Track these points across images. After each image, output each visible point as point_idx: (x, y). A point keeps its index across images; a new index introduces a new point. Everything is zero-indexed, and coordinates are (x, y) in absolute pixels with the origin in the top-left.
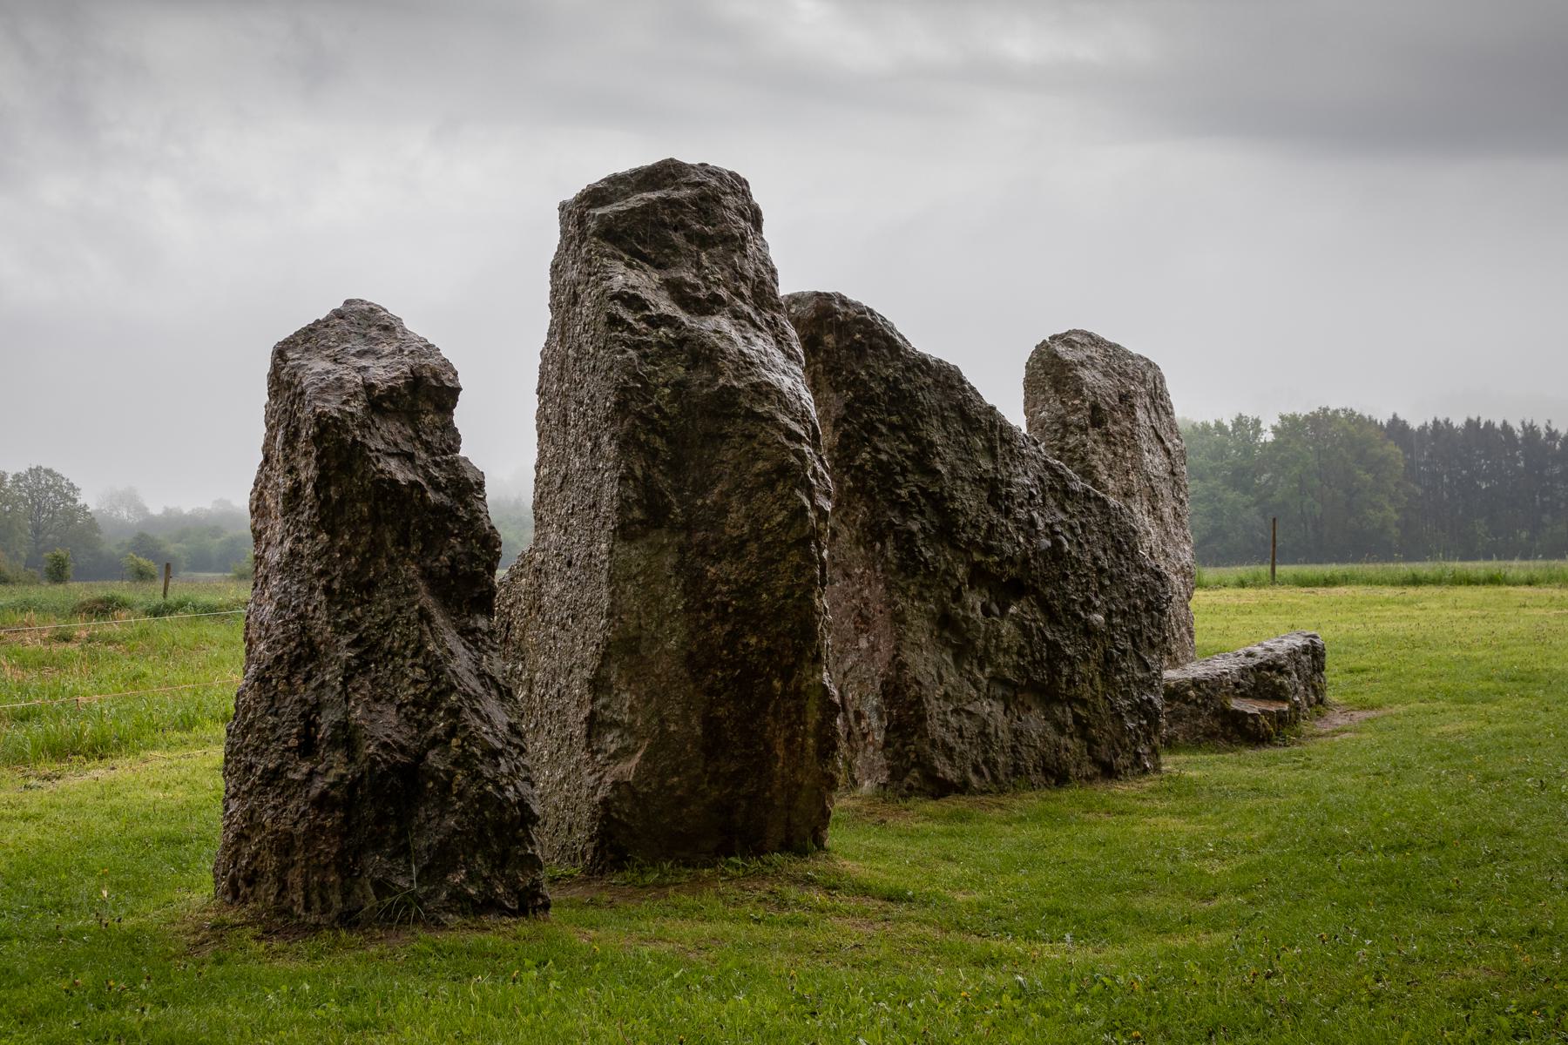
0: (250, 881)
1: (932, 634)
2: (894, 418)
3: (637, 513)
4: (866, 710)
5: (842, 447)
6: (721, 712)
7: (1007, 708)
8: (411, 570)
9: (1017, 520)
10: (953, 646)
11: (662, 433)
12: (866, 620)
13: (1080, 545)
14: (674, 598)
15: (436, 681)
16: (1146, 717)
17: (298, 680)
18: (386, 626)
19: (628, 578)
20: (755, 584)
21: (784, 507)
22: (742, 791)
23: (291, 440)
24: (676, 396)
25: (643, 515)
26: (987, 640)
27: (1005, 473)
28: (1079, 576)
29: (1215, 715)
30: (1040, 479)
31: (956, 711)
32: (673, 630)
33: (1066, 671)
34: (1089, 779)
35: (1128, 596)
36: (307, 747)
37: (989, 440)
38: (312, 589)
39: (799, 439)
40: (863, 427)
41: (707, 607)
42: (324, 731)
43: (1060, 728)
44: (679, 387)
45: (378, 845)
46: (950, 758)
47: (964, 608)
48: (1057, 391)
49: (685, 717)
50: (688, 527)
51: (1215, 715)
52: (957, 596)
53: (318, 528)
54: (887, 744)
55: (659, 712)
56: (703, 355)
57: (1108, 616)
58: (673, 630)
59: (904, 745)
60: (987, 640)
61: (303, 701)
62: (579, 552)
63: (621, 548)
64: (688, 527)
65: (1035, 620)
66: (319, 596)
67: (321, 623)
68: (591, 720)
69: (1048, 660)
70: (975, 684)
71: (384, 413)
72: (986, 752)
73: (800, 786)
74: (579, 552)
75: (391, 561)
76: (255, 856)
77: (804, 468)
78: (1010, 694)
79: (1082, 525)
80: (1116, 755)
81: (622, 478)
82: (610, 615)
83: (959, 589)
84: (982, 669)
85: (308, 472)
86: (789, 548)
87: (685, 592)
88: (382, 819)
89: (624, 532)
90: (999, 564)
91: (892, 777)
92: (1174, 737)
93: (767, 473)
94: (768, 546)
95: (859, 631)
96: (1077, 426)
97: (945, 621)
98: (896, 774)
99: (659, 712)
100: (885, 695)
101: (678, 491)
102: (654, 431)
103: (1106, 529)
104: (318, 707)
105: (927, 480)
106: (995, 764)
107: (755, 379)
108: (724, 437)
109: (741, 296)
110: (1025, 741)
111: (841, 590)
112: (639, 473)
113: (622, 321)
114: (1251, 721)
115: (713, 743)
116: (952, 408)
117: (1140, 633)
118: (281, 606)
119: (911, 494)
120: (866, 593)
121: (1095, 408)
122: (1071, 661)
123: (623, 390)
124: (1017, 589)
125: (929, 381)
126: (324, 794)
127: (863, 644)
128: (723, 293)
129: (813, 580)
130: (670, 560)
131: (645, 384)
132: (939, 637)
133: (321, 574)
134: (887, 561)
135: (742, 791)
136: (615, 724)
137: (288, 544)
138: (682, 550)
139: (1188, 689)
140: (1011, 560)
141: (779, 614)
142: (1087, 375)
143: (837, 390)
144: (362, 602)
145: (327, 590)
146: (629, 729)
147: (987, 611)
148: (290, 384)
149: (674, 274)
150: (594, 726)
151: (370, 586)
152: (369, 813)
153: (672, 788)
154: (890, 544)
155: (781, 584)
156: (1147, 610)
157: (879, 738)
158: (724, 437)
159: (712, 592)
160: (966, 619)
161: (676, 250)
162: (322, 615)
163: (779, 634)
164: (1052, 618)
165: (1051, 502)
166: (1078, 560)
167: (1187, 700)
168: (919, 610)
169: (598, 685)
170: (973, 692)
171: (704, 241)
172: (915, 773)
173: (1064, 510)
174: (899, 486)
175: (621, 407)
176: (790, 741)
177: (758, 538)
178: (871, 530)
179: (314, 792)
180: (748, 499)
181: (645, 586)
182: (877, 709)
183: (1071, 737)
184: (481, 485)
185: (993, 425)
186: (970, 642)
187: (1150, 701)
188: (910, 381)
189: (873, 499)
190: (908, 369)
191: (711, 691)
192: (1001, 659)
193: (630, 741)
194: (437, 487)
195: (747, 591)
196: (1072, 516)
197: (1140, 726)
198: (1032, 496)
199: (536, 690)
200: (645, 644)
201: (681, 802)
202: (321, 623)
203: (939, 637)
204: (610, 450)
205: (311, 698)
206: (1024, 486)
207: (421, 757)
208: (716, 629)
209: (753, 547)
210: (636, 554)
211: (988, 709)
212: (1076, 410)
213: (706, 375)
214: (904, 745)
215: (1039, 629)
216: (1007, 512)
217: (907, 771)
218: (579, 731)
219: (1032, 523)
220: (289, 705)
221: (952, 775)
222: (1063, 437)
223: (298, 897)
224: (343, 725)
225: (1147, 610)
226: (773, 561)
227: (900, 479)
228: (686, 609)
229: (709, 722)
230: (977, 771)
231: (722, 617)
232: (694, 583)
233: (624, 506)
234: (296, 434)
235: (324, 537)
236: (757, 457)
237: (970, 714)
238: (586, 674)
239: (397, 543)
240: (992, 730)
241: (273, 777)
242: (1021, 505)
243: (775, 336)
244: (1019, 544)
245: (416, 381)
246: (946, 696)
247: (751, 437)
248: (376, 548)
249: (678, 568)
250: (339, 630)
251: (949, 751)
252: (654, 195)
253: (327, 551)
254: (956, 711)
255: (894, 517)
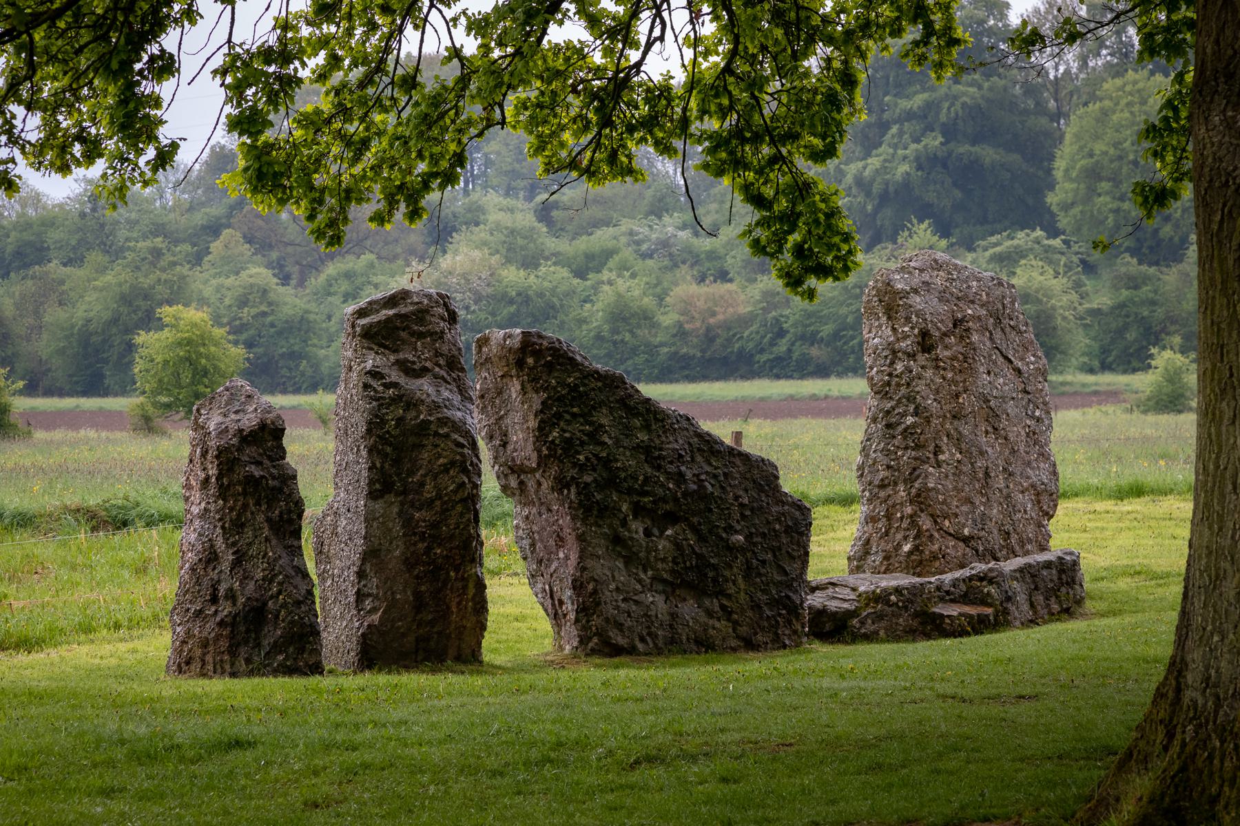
0: (188, 663)
1: (607, 548)
2: (575, 410)
3: (378, 486)
4: (565, 598)
5: (540, 429)
6: (423, 588)
7: (667, 598)
8: (261, 518)
9: (667, 473)
10: (624, 557)
11: (391, 445)
12: (562, 539)
13: (722, 488)
14: (398, 529)
15: (273, 570)
16: (784, 608)
17: (209, 570)
18: (250, 544)
19: (374, 519)
20: (439, 522)
21: (454, 482)
22: (435, 630)
23: (204, 454)
24: (397, 426)
25: (381, 485)
26: (649, 552)
27: (657, 442)
28: (722, 510)
29: (916, 615)
30: (690, 444)
31: (624, 600)
32: (398, 546)
33: (711, 574)
34: (734, 650)
35: (768, 522)
36: (214, 600)
37: (646, 420)
38: (215, 527)
39: (463, 446)
40: (554, 416)
41: (415, 534)
42: (222, 592)
43: (710, 614)
44: (400, 420)
45: (246, 642)
46: (621, 631)
47: (629, 531)
48: (889, 318)
49: (404, 591)
50: (404, 493)
51: (916, 615)
52: (624, 523)
53: (218, 497)
54: (577, 621)
55: (391, 588)
56: (411, 403)
57: (749, 537)
58: (398, 546)
59: (588, 621)
60: (649, 552)
61: (212, 579)
62: (353, 504)
63: (371, 504)
64: (404, 493)
65: (686, 540)
66: (219, 530)
67: (220, 544)
68: (358, 593)
69: (697, 566)
70: (640, 581)
71: (249, 444)
72: (649, 627)
73: (465, 627)
74: (353, 504)
75: (252, 513)
76: (190, 651)
77: (465, 462)
78: (669, 589)
79: (725, 474)
80: (755, 634)
81: (370, 468)
82: (365, 538)
83: (625, 519)
84: (645, 572)
85: (213, 471)
86: (457, 503)
87: (403, 526)
88: (248, 631)
89: (373, 495)
90: (654, 502)
91: (581, 642)
92: (876, 633)
93: (445, 465)
94: (445, 503)
95: (559, 547)
96: (905, 353)
97: (617, 540)
98: (583, 641)
99: (391, 588)
100: (574, 588)
101: (398, 475)
102: (386, 444)
103: (748, 476)
104: (219, 581)
105: (599, 448)
106: (657, 636)
107: (440, 415)
108: (424, 446)
109: (440, 366)
110: (679, 621)
111: (546, 520)
112: (378, 465)
113: (371, 386)
114: (947, 621)
115: (419, 604)
116: (617, 401)
117: (780, 549)
118: (200, 535)
119: (587, 459)
120: (561, 522)
121: (925, 334)
122: (715, 567)
123: (370, 423)
124: (672, 518)
125: (599, 384)
126: (222, 620)
127: (561, 555)
128: (428, 364)
129: (469, 520)
130: (395, 510)
131: (382, 420)
132: (613, 550)
133: (220, 520)
134: (571, 502)
135: (435, 630)
136: (369, 595)
137: (203, 505)
138: (402, 504)
139: (891, 594)
140: (664, 500)
141: (452, 537)
142: (916, 301)
143: (537, 392)
144: (238, 533)
145: (223, 527)
146: (376, 597)
147: (648, 533)
148: (203, 428)
149: (401, 356)
150: (360, 596)
151: (243, 525)
152: (242, 628)
153: (399, 628)
154: (573, 490)
155: (452, 521)
156: (786, 532)
157: (572, 616)
158: (424, 446)
159: (417, 526)
160: (631, 539)
161: (404, 342)
162: (220, 539)
163: (452, 548)
164: (702, 539)
165: (699, 458)
166: (721, 498)
167: (888, 603)
168: (595, 532)
169: (361, 574)
170: (638, 587)
171: (421, 336)
172: (595, 640)
173: (710, 464)
174: (579, 453)
175: (369, 431)
176: (459, 603)
177: (441, 498)
178: (560, 481)
179: (218, 619)
180: (435, 477)
181: (383, 523)
182: (570, 597)
183: (719, 620)
184: (295, 477)
185: (648, 411)
186: (636, 554)
187: (788, 597)
188: (585, 385)
189: (562, 461)
190: (585, 377)
191: (417, 577)
192: (660, 565)
193: (377, 603)
194: (274, 478)
195: (435, 525)
196: (716, 468)
197: (780, 615)
198: (681, 456)
199: (336, 579)
200: (383, 553)
201: (404, 635)
202: (220, 544)
203: (613, 550)
204: (364, 453)
205: (216, 578)
206: (674, 450)
207: (265, 604)
208: (420, 545)
209: (438, 503)
210: (379, 506)
211: (651, 599)
212: (906, 337)
213: (414, 414)
214: (588, 621)
215: (690, 545)
216: (659, 468)
217: (590, 639)
218: (352, 599)
219: (681, 474)
220: (206, 582)
221: (621, 641)
222: (892, 363)
223: (211, 667)
224: (231, 589)
225: (786, 532)
226: (447, 510)
227: (580, 449)
228: (404, 535)
229: (417, 595)
230: (642, 640)
231: (423, 539)
232: (408, 523)
233: (371, 483)
234: (207, 452)
235: (221, 502)
236: (440, 456)
237: (636, 602)
238: (356, 569)
239: (255, 505)
240: (653, 613)
241: (199, 613)
242: (671, 463)
243: (458, 387)
244: (669, 489)
245: (263, 426)
246: (617, 589)
247: (437, 446)
248: (245, 506)
249: (400, 514)
250: (228, 547)
251: (620, 626)
252: (391, 312)
253: (223, 509)
254: (624, 600)
255: (573, 472)
